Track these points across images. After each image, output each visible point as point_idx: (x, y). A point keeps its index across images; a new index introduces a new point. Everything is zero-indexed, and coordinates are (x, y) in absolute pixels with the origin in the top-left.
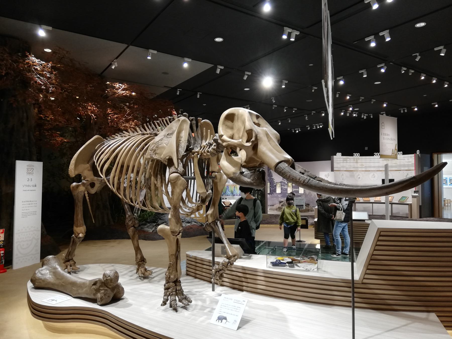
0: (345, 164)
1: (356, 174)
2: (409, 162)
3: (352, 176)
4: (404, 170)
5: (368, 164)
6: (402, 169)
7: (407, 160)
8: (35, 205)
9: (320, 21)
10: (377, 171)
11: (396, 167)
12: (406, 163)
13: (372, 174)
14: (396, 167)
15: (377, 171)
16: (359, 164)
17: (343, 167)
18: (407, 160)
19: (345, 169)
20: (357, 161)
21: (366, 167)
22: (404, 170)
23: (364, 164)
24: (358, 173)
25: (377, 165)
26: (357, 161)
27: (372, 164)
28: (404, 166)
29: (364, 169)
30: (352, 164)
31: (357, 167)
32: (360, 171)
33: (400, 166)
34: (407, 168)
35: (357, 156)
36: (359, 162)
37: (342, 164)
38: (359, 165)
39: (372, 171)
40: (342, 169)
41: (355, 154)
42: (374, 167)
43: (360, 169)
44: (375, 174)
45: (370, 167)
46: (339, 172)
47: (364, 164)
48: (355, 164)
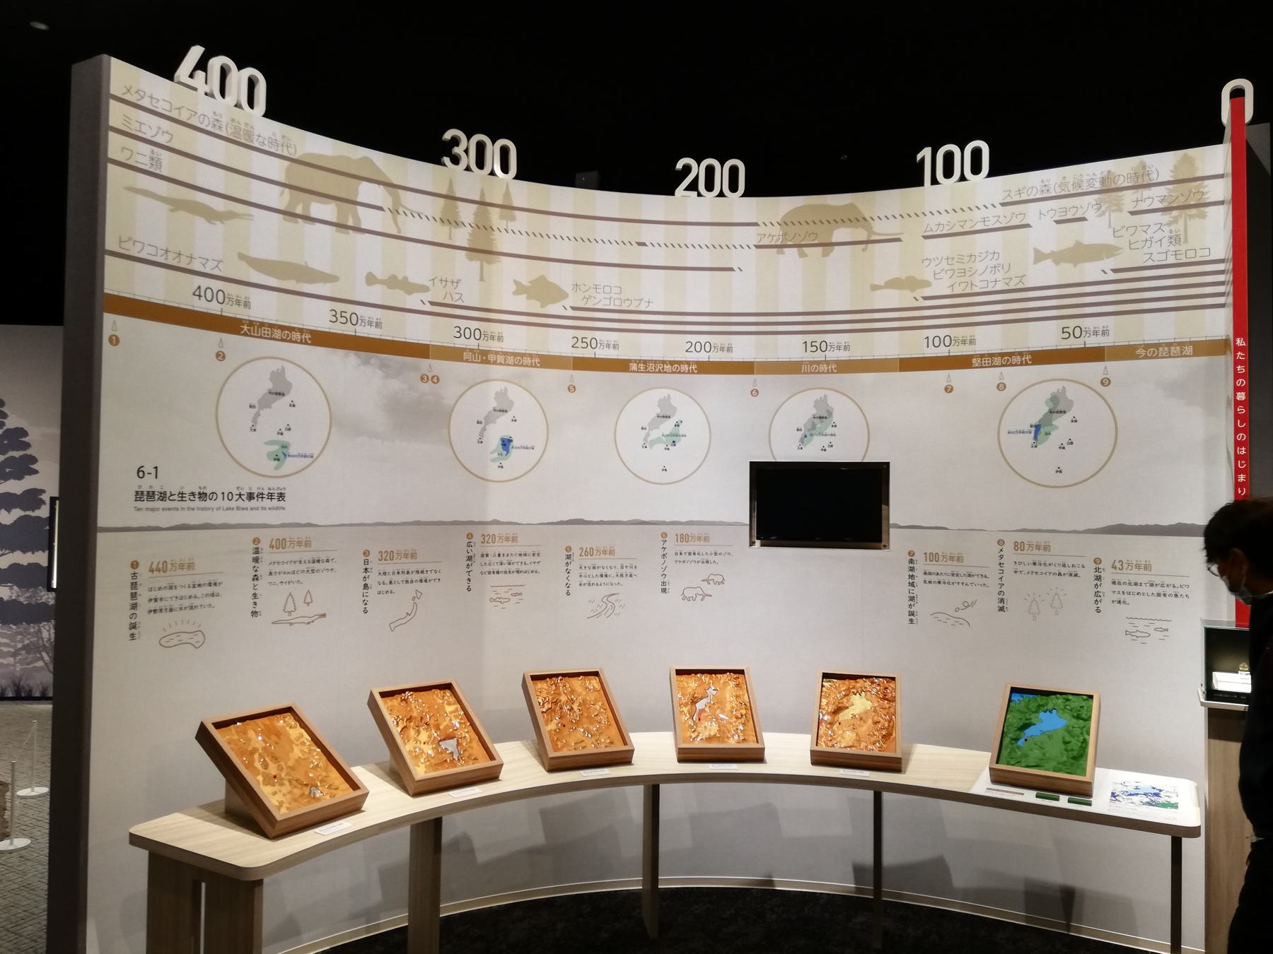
0: (317, 246)
1: (470, 393)
2: (1081, 253)
3: (421, 418)
4: (1007, 358)
5: (607, 288)
6: (989, 339)
7: (1044, 231)
8: (486, 560)
9: (269, 275)
10: (706, 368)
11: (905, 320)
12: (1046, 274)
13: (646, 398)
14: (905, 320)
15: (706, 368)
16: (508, 273)
17: (292, 277)
18: (1044, 231)
19: (318, 317)
20: (483, 227)
21: (584, 319)
22: (1007, 358)
23: (560, 276)
24: (498, 380)
25: (698, 294)
26: (483, 227)
27: (654, 292)
28: (1016, 303)
29: (561, 343)
30: (418, 264)
31: (485, 314)
32: (518, 358)
33: (964, 307)
34: (1046, 336)
35: (480, 175)
36: (503, 242)
37: (266, 236)
38: (504, 285)
39: (648, 366)
40: (264, 307)
41: (466, 146)
42: (675, 322)
43: (515, 339)
44: (688, 413)
45: (630, 319)
46: (211, 339)
47: (560, 276)
48: (464, 266)
